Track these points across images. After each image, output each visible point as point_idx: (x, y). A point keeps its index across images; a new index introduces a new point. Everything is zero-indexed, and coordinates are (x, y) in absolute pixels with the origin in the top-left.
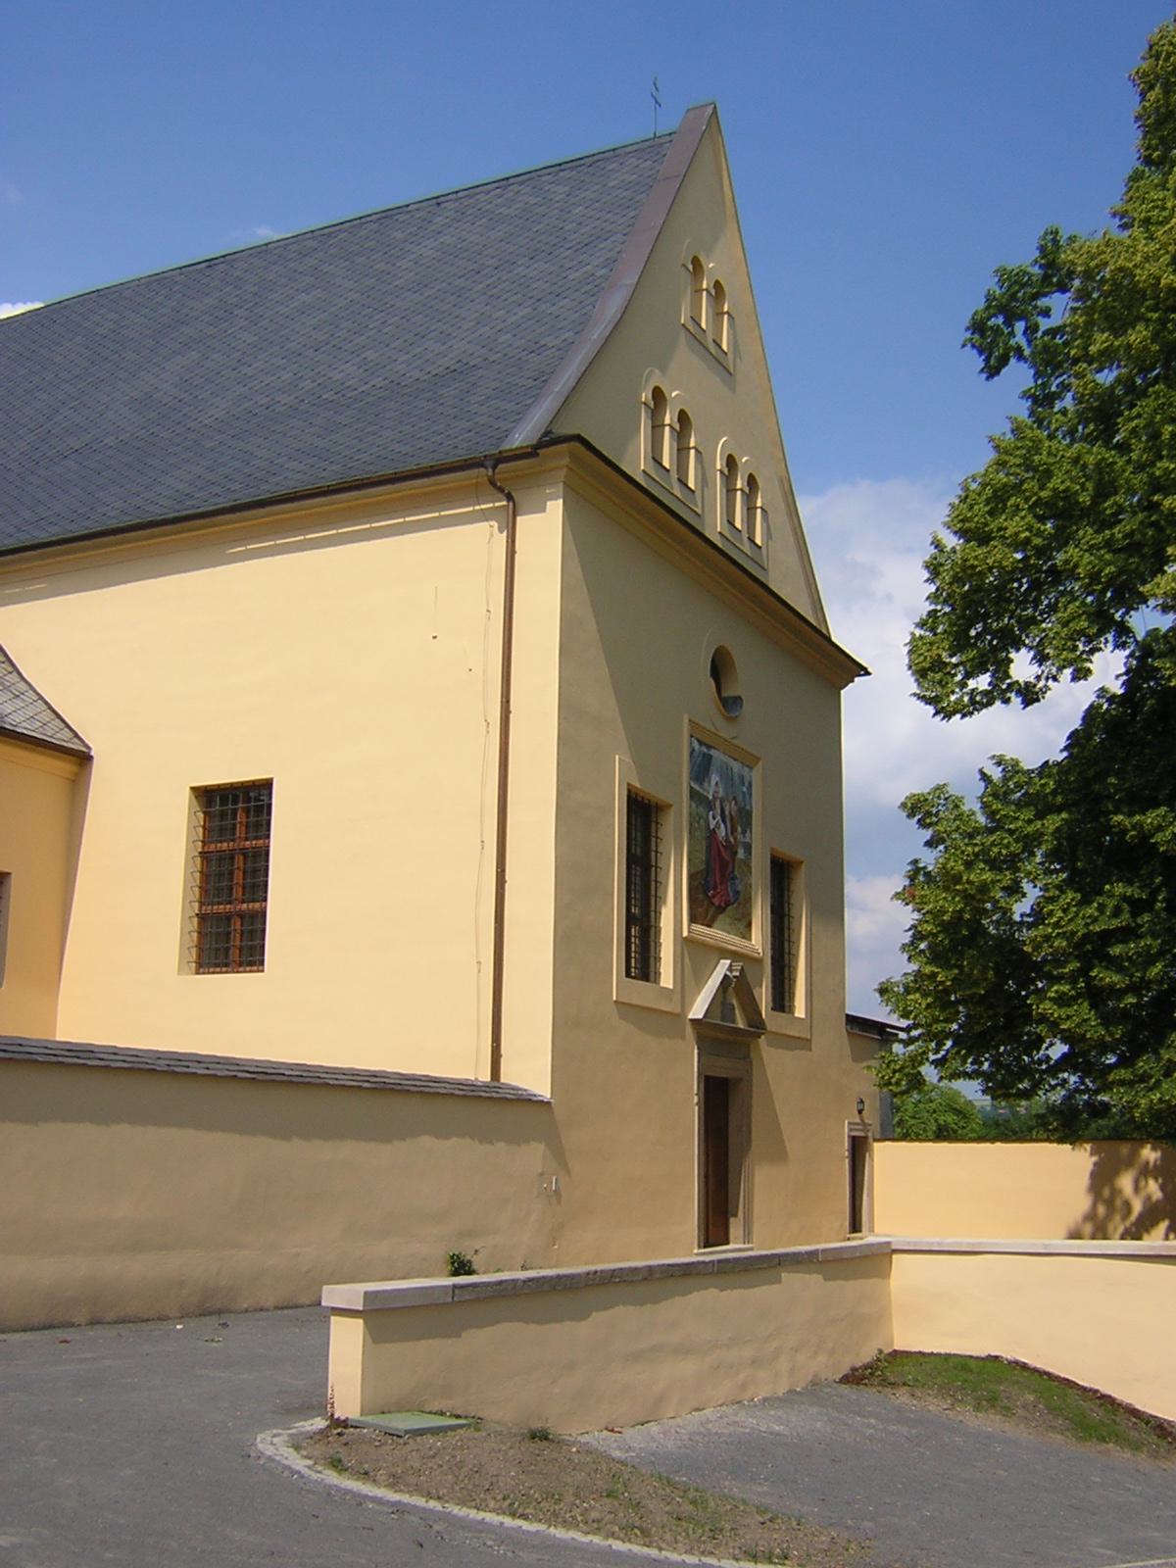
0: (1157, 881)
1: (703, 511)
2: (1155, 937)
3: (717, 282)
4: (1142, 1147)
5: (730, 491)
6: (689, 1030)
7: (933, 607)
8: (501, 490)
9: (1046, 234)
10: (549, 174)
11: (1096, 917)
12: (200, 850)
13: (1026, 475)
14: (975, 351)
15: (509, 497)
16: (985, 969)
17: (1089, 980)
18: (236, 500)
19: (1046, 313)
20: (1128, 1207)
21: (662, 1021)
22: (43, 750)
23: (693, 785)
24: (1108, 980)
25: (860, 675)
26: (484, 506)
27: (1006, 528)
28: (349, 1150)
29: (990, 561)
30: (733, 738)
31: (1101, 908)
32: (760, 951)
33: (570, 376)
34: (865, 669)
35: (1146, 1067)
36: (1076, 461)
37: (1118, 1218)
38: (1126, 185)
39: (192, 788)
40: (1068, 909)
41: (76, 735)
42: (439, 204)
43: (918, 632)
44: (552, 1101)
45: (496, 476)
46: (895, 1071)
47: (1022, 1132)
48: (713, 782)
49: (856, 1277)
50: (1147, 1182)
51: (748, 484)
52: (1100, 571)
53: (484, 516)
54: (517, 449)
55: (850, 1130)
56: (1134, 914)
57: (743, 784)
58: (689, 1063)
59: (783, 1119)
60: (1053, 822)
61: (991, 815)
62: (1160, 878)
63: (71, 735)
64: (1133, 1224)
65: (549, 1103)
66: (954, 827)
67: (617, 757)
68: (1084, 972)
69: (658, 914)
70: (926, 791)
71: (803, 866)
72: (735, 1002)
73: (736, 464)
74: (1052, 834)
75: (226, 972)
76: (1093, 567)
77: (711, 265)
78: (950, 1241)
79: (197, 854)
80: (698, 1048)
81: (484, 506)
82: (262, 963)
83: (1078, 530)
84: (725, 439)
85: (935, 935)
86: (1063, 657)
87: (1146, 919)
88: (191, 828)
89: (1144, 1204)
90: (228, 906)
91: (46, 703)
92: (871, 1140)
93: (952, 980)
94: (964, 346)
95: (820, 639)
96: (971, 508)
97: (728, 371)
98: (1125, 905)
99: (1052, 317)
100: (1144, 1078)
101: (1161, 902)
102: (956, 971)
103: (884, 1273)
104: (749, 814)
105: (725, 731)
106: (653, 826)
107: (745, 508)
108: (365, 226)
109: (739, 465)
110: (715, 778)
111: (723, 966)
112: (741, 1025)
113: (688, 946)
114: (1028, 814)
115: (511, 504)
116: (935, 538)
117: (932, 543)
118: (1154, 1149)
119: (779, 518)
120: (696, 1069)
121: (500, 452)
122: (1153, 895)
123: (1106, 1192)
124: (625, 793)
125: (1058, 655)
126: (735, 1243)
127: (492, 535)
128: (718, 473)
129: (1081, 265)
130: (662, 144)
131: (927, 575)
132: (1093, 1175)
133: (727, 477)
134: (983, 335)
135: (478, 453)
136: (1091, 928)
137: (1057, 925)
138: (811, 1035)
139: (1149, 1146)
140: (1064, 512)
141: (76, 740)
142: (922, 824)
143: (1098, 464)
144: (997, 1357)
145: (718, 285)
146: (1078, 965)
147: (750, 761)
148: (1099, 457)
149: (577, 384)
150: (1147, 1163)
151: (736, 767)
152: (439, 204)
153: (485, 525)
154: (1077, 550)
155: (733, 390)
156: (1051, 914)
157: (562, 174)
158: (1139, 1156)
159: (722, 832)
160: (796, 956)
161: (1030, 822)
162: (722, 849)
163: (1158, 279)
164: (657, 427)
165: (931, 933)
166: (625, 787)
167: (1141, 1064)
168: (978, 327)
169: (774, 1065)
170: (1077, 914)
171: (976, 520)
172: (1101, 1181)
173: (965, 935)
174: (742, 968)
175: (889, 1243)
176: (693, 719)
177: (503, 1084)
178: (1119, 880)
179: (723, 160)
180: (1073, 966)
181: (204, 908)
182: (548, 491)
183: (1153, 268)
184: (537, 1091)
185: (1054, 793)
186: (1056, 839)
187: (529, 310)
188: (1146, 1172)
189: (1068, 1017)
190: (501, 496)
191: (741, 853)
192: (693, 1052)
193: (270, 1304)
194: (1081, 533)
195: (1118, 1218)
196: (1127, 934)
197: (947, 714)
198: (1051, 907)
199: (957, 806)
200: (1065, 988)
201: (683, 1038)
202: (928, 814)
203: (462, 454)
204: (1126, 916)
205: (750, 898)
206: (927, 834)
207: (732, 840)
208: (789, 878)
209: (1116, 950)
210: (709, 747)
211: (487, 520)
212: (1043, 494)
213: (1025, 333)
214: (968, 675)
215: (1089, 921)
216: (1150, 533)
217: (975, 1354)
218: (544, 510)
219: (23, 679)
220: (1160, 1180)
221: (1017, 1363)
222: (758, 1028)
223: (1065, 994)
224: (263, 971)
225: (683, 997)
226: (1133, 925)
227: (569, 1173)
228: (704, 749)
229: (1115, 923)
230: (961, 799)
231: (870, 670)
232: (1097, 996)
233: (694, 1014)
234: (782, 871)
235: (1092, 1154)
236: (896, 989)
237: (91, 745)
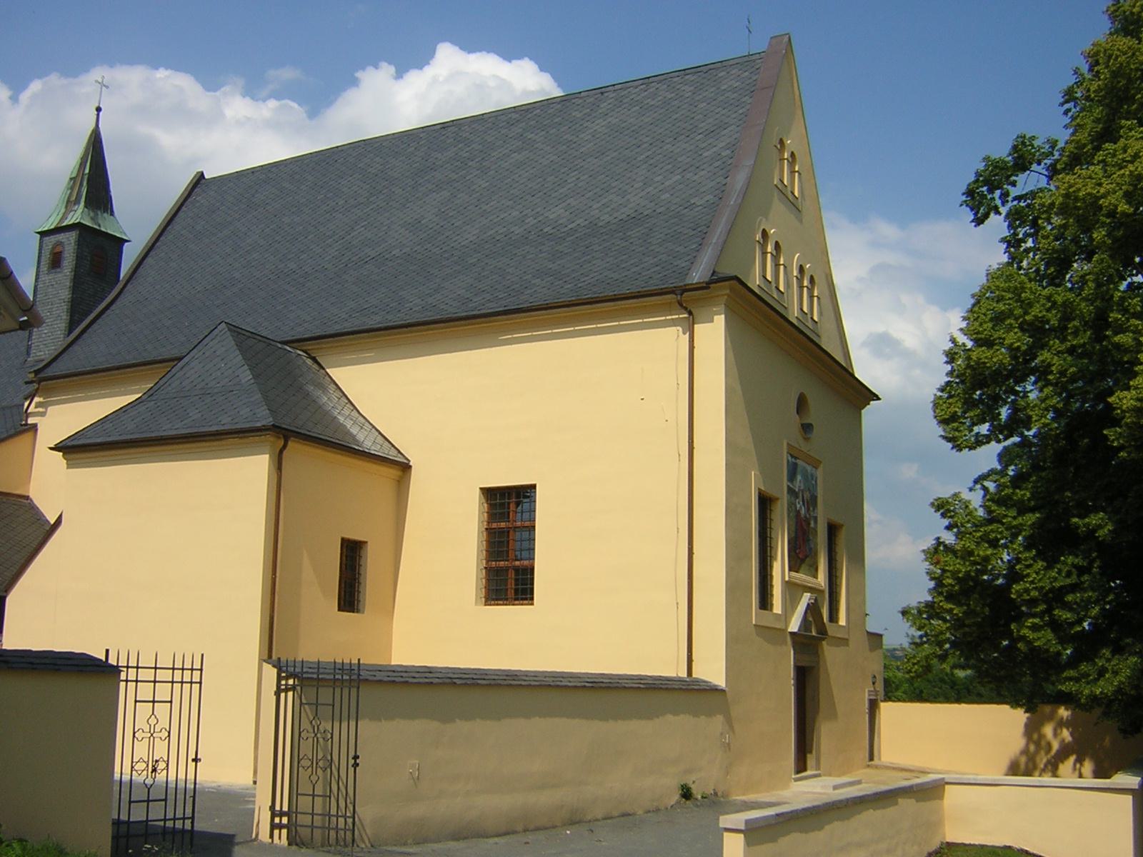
0: (1093, 555)
1: (788, 305)
2: (1093, 590)
3: (792, 153)
4: (1059, 708)
5: (801, 287)
6: (789, 639)
7: (949, 379)
8: (686, 308)
9: (1018, 137)
10: (678, 76)
11: (1056, 577)
12: (485, 527)
13: (1015, 305)
14: (968, 209)
15: (690, 313)
16: (984, 605)
17: (1051, 615)
19: (1014, 184)
20: (1049, 745)
21: (771, 633)
22: (359, 457)
23: (789, 484)
24: (1064, 616)
25: (874, 400)
26: (674, 317)
27: (1004, 339)
28: (635, 725)
29: (995, 360)
30: (809, 451)
31: (1059, 572)
32: (823, 585)
33: (721, 232)
34: (877, 396)
35: (1086, 669)
36: (1049, 298)
37: (1043, 753)
38: (1063, 97)
39: (481, 489)
40: (1039, 572)
41: (399, 452)
42: (602, 93)
43: (939, 394)
44: (727, 689)
45: (683, 299)
46: (914, 664)
47: (935, 682)
48: (798, 480)
49: (929, 799)
50: (1062, 730)
51: (776, 249)
52: (1066, 370)
53: (673, 323)
54: (696, 283)
55: (869, 695)
56: (1079, 576)
57: (812, 479)
58: (789, 658)
59: (835, 691)
60: (1031, 518)
61: (990, 512)
62: (1096, 554)
63: (396, 452)
64: (1053, 757)
65: (723, 691)
66: (966, 519)
67: (753, 473)
68: (1049, 611)
69: (771, 567)
70: (947, 496)
71: (844, 528)
72: (811, 619)
73: (767, 235)
74: (1030, 526)
75: (506, 605)
76: (1062, 367)
77: (789, 142)
78: (981, 778)
79: (484, 530)
80: (794, 650)
81: (674, 317)
82: (532, 599)
83: (1050, 340)
84: (798, 254)
85: (953, 586)
86: (1042, 421)
87: (1086, 578)
88: (481, 513)
89: (1060, 746)
90: (506, 563)
91: (377, 430)
92: (879, 701)
93: (963, 613)
94: (961, 205)
95: (848, 376)
96: (981, 325)
97: (799, 210)
98: (1074, 570)
99: (1018, 186)
100: (1086, 675)
101: (1096, 568)
102: (965, 608)
103: (941, 797)
104: (816, 497)
105: (804, 447)
107: (773, 265)
108: (551, 106)
109: (806, 270)
110: (799, 478)
111: (807, 596)
112: (814, 634)
113: (789, 586)
114: (1013, 513)
115: (691, 317)
116: (952, 336)
117: (950, 340)
118: (1066, 709)
119: (826, 301)
120: (792, 663)
121: (685, 285)
122: (1091, 563)
123: (1035, 736)
124: (757, 492)
125: (1039, 420)
126: (811, 770)
127: (678, 336)
128: (795, 278)
129: (1064, 190)
130: (754, 61)
131: (945, 359)
132: (1026, 725)
133: (762, 245)
134: (973, 198)
135: (669, 285)
136: (1054, 584)
137: (1032, 582)
138: (849, 636)
139: (1063, 708)
140: (1038, 331)
141: (399, 455)
142: (943, 515)
143: (1064, 303)
144: (1010, 847)
145: (792, 155)
146: (1045, 606)
147: (816, 464)
148: (1065, 298)
149: (727, 237)
150: (1062, 718)
151: (809, 468)
152: (602, 93)
153: (674, 329)
154: (1049, 353)
155: (801, 221)
156: (1028, 575)
157: (687, 77)
158: (1057, 712)
159: (803, 512)
160: (841, 583)
161: (1014, 518)
163: (1116, 207)
164: (764, 253)
165: (951, 585)
166: (757, 489)
167: (1083, 667)
168: (970, 193)
169: (830, 653)
170: (1044, 575)
171: (985, 333)
172: (1032, 730)
173: (971, 586)
174: (816, 598)
175: (943, 779)
176: (790, 443)
177: (695, 678)
178: (1070, 554)
179: (794, 68)
180: (1042, 607)
181: (490, 563)
182: (714, 309)
183: (1112, 199)
184: (720, 684)
185: (1029, 500)
186: (1032, 529)
187: (679, 177)
188: (1061, 724)
189: (1039, 638)
190: (683, 311)
191: (812, 522)
192: (790, 652)
193: (600, 817)
194: (1051, 342)
195: (1043, 753)
196: (1073, 588)
197: (959, 448)
198: (1028, 571)
199: (967, 507)
200: (1037, 620)
201: (786, 644)
202: (949, 511)
203: (654, 285)
204: (1074, 576)
205: (817, 551)
206: (946, 522)
207: (808, 516)
208: (835, 536)
209: (1069, 598)
210: (796, 458)
211: (675, 326)
212: (1027, 318)
213: (1000, 198)
214: (974, 424)
215: (1052, 580)
216: (1098, 347)
217: (997, 844)
218: (713, 322)
219: (361, 414)
220: (1070, 730)
221: (1022, 850)
222: (823, 634)
223: (1037, 624)
224: (532, 604)
225: (786, 618)
226: (1078, 582)
227: (734, 732)
228: (793, 460)
229: (1068, 581)
230: (969, 502)
231: (880, 397)
232: (1055, 625)
233: (792, 628)
234: (833, 530)
235: (1026, 712)
236: (912, 612)
237: (409, 458)
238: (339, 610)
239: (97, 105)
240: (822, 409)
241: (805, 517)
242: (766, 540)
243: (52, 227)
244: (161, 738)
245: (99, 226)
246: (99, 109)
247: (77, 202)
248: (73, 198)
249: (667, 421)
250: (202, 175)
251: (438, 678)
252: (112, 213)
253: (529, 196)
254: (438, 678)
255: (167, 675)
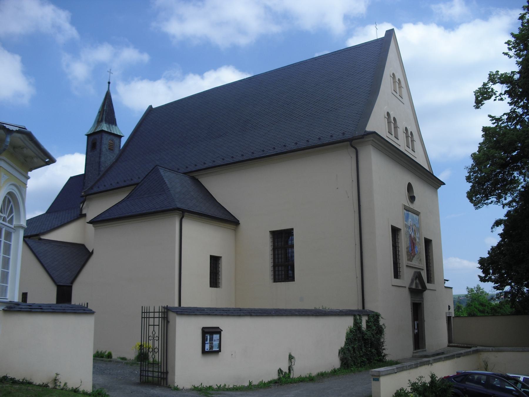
18: (276, 152)
25: (442, 185)
48: (410, 221)
105: (411, 206)
106: (397, 235)
159: (412, 235)
162: (413, 239)
207: (415, 237)
231: (445, 183)
238: (210, 287)
239: (108, 81)
240: (419, 189)
241: (414, 237)
242: (396, 240)
243: (92, 132)
244: (156, 340)
245: (111, 131)
246: (109, 83)
247: (102, 121)
248: (100, 120)
249: (348, 197)
250: (151, 106)
251: (244, 313)
252: (116, 125)
253: (286, 105)
254: (244, 313)
255: (152, 315)
